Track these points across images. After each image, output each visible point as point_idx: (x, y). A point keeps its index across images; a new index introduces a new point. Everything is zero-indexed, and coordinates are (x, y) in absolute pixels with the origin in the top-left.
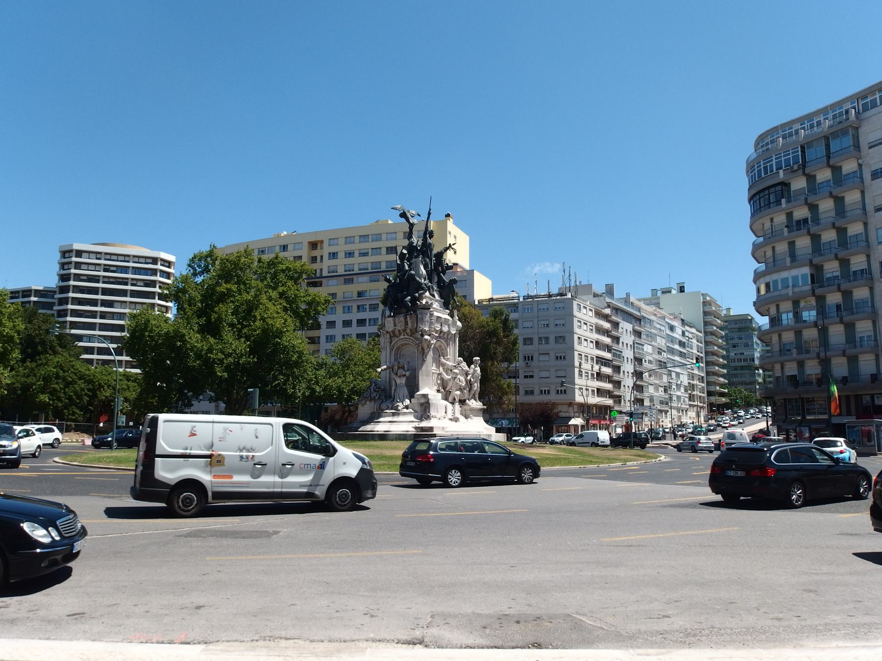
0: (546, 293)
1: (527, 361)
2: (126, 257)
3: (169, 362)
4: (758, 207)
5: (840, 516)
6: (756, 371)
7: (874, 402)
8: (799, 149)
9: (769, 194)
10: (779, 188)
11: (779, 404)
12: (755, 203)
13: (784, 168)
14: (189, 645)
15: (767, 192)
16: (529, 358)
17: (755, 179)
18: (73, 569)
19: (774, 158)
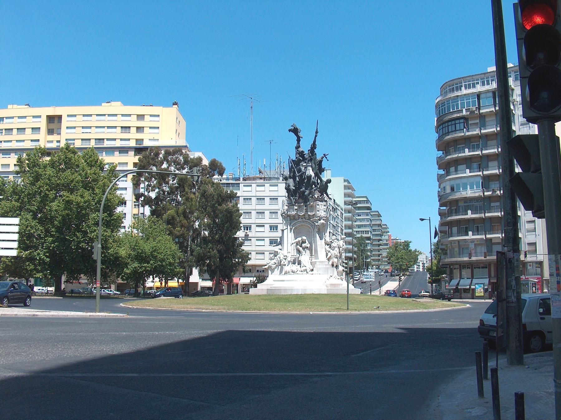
0: (460, 124)
1: (246, 231)
2: (176, 315)
3: (80, 251)
4: (447, 131)
5: (404, 325)
6: (210, 243)
7: (541, 270)
8: (476, 96)
9: (448, 126)
10: (462, 121)
11: (60, 246)
12: (440, 131)
13: (466, 108)
14: (152, 107)
15: (453, 122)
16: (248, 228)
17: (445, 112)
18: (289, 129)
19: (446, 103)
